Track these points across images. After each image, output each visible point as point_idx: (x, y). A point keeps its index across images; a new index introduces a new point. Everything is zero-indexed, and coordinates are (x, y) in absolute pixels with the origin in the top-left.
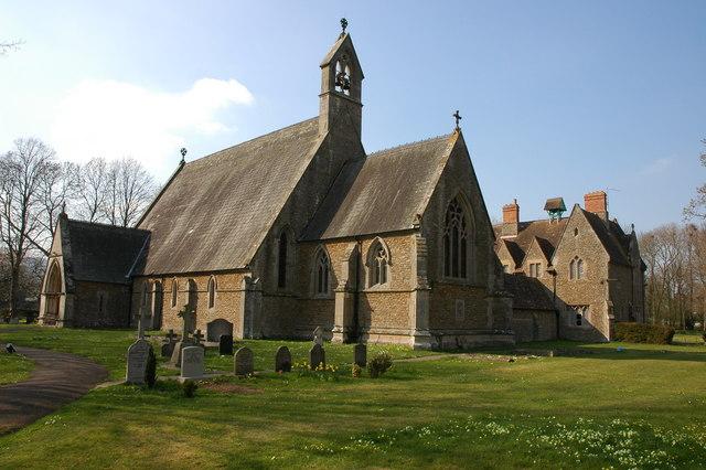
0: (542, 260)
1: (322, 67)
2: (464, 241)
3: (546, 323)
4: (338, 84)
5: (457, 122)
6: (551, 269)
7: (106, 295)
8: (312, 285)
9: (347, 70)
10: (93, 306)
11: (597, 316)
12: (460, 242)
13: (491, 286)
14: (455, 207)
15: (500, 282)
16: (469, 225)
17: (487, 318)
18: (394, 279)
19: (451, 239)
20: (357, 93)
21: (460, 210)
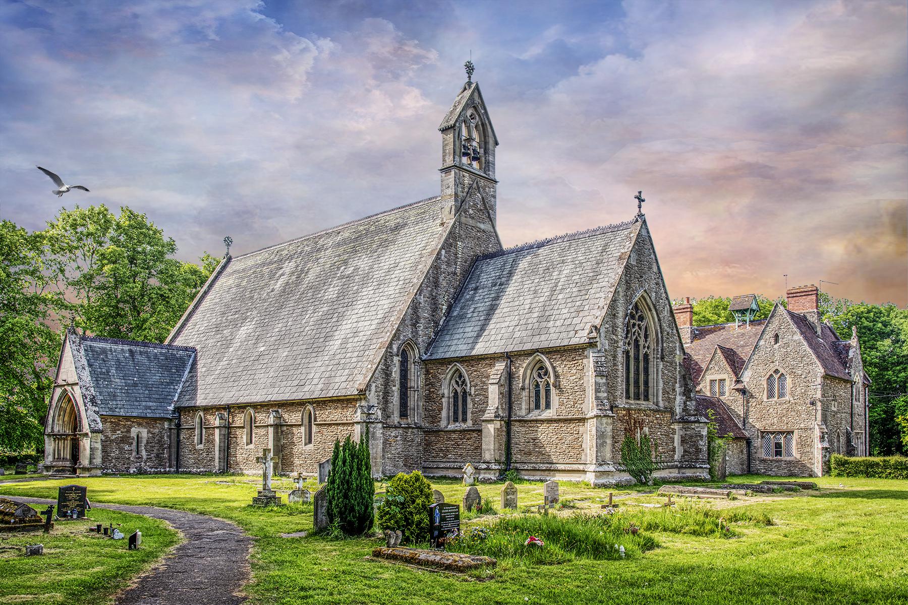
0: (728, 376)
1: (444, 130)
2: (646, 356)
3: (730, 455)
4: (465, 154)
5: (640, 207)
6: (739, 386)
7: (144, 433)
8: (444, 413)
9: (475, 135)
10: (127, 447)
11: (804, 444)
12: (641, 357)
13: (678, 410)
14: (636, 314)
15: (692, 405)
16: (652, 335)
17: (674, 450)
18: (561, 404)
19: (632, 354)
20: (488, 166)
21: (641, 318)
